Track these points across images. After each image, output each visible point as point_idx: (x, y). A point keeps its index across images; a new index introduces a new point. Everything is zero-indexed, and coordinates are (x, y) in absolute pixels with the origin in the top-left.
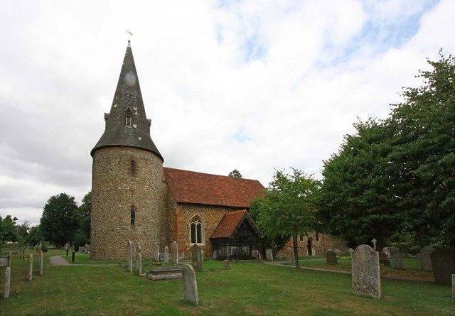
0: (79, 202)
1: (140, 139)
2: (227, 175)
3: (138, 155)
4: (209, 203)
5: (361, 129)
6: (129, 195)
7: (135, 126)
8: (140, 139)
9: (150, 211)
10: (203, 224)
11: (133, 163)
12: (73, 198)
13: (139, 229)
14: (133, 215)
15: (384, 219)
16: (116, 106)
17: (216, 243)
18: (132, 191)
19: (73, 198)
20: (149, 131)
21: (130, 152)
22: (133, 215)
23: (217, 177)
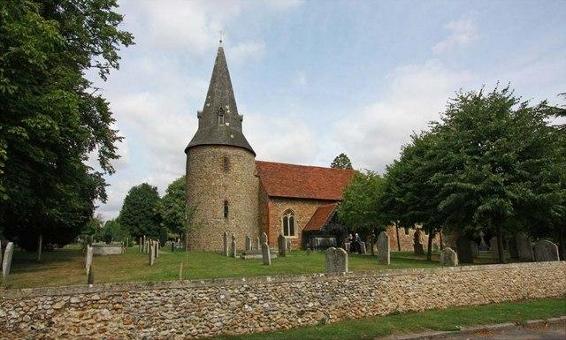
0: (162, 193)
1: (232, 136)
2: (328, 166)
3: (230, 152)
4: (302, 197)
5: (417, 141)
6: (222, 190)
7: (227, 124)
8: (232, 136)
9: (243, 208)
10: (296, 218)
11: (226, 160)
12: (156, 188)
13: (232, 222)
14: (226, 209)
15: (173, 233)
16: (208, 105)
17: (307, 236)
18: (225, 187)
19: (156, 188)
20: (241, 127)
21: (223, 150)
22: (226, 209)
23: (312, 168)
